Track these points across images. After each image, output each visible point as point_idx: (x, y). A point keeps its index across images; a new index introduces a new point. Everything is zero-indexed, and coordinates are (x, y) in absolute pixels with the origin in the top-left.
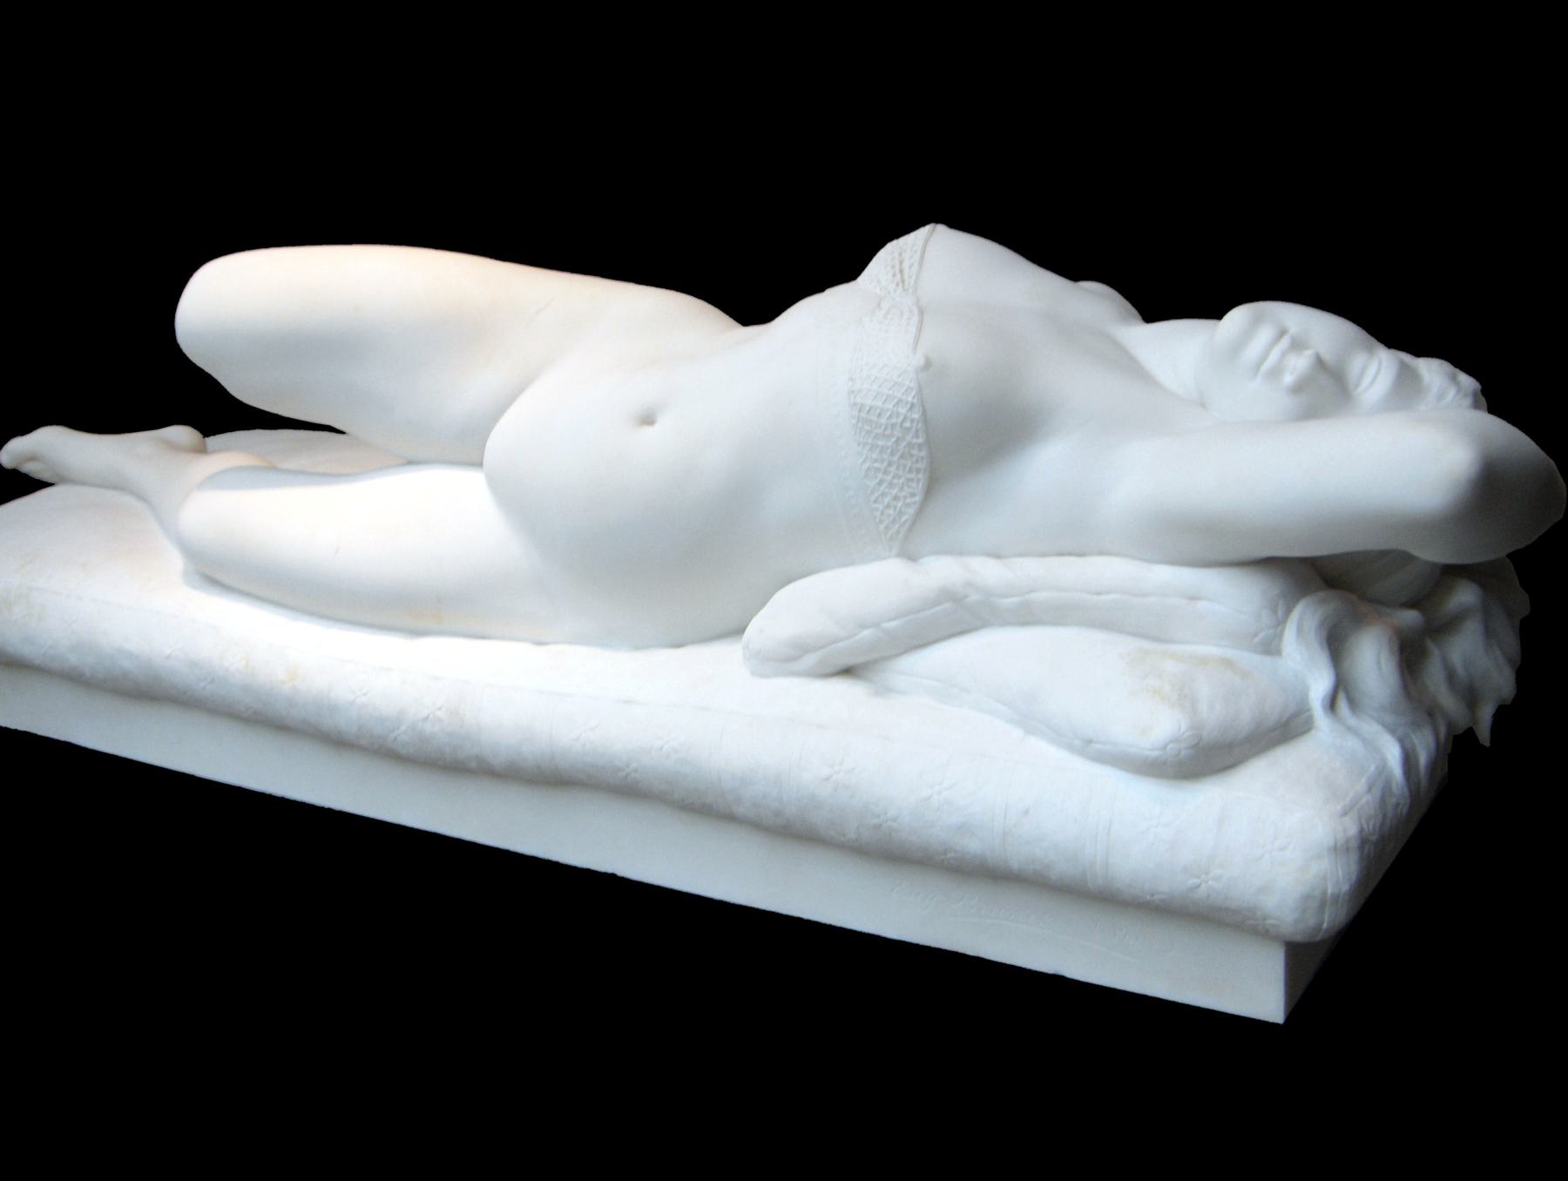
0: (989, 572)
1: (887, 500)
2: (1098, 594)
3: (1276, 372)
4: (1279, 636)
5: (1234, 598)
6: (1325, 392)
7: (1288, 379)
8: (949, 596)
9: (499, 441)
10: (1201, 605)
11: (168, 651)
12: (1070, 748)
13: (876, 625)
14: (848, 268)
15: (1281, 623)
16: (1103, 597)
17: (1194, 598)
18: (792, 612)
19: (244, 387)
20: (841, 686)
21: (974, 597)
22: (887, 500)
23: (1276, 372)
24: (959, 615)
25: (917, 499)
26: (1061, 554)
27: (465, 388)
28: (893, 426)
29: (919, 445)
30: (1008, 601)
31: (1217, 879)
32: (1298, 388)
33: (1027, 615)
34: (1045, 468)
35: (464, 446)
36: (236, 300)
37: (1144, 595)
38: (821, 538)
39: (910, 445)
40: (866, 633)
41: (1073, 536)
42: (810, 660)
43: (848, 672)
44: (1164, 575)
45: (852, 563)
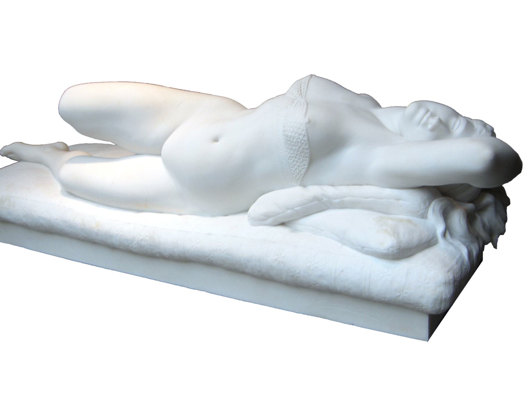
0: (330, 191)
1: (296, 167)
2: (366, 198)
3: (425, 124)
4: (427, 212)
5: (412, 200)
7: (430, 126)
8: (316, 199)
9: (166, 147)
10: (401, 202)
11: (56, 217)
12: (357, 249)
13: (292, 209)
14: (510, 180)
15: (427, 208)
16: (368, 199)
17: (398, 200)
18: (264, 204)
20: (281, 229)
21: (325, 199)
22: (296, 167)
23: (425, 124)
24: (320, 205)
25: (306, 166)
26: (354, 185)
28: (298, 142)
29: (307, 148)
30: (336, 200)
31: (406, 293)
32: (433, 130)
33: (343, 205)
34: (348, 156)
35: (155, 149)
37: (382, 199)
38: (274, 179)
39: (303, 149)
40: (289, 211)
41: (358, 179)
42: (270, 220)
43: (283, 224)
44: (388, 192)
45: (284, 188)
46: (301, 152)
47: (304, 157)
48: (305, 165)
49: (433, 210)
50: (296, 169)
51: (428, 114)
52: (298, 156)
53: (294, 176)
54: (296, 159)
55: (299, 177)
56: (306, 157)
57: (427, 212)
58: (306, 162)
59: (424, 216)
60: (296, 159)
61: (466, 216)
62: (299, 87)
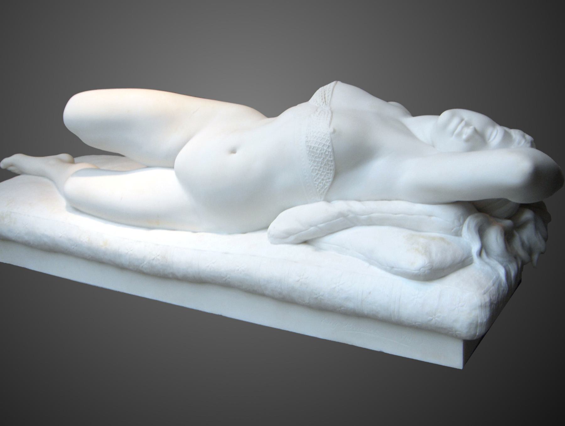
0: (356, 206)
1: (319, 180)
2: (396, 214)
3: (460, 134)
4: (461, 230)
5: (445, 216)
6: (477, 141)
7: (464, 137)
8: (342, 215)
9: (180, 159)
10: (433, 218)
11: (61, 235)
12: (386, 270)
13: (316, 226)
15: (462, 225)
16: (397, 216)
17: (430, 216)
18: (285, 221)
19: (87, 139)
20: (303, 247)
21: (351, 215)
22: (319, 180)
23: (460, 134)
24: (346, 222)
25: (330, 180)
27: (168, 140)
28: (322, 153)
29: (331, 161)
30: (363, 217)
31: (438, 317)
32: (468, 140)
33: (370, 222)
34: (376, 169)
35: (167, 161)
36: (85, 107)
37: (412, 215)
38: (296, 194)
39: (328, 161)
40: (312, 228)
41: (387, 194)
42: (292, 238)
43: (305, 242)
44: (420, 207)
45: (307, 203)
46: (325, 165)
47: (328, 170)
48: (329, 179)
49: (468, 227)
50: (320, 183)
51: (463, 124)
52: (322, 169)
53: (318, 190)
54: (320, 172)
55: (324, 192)
56: (331, 170)
57: (461, 229)
58: (331, 176)
59: (458, 234)
60: (320, 172)
61: (503, 234)
62: (323, 95)
